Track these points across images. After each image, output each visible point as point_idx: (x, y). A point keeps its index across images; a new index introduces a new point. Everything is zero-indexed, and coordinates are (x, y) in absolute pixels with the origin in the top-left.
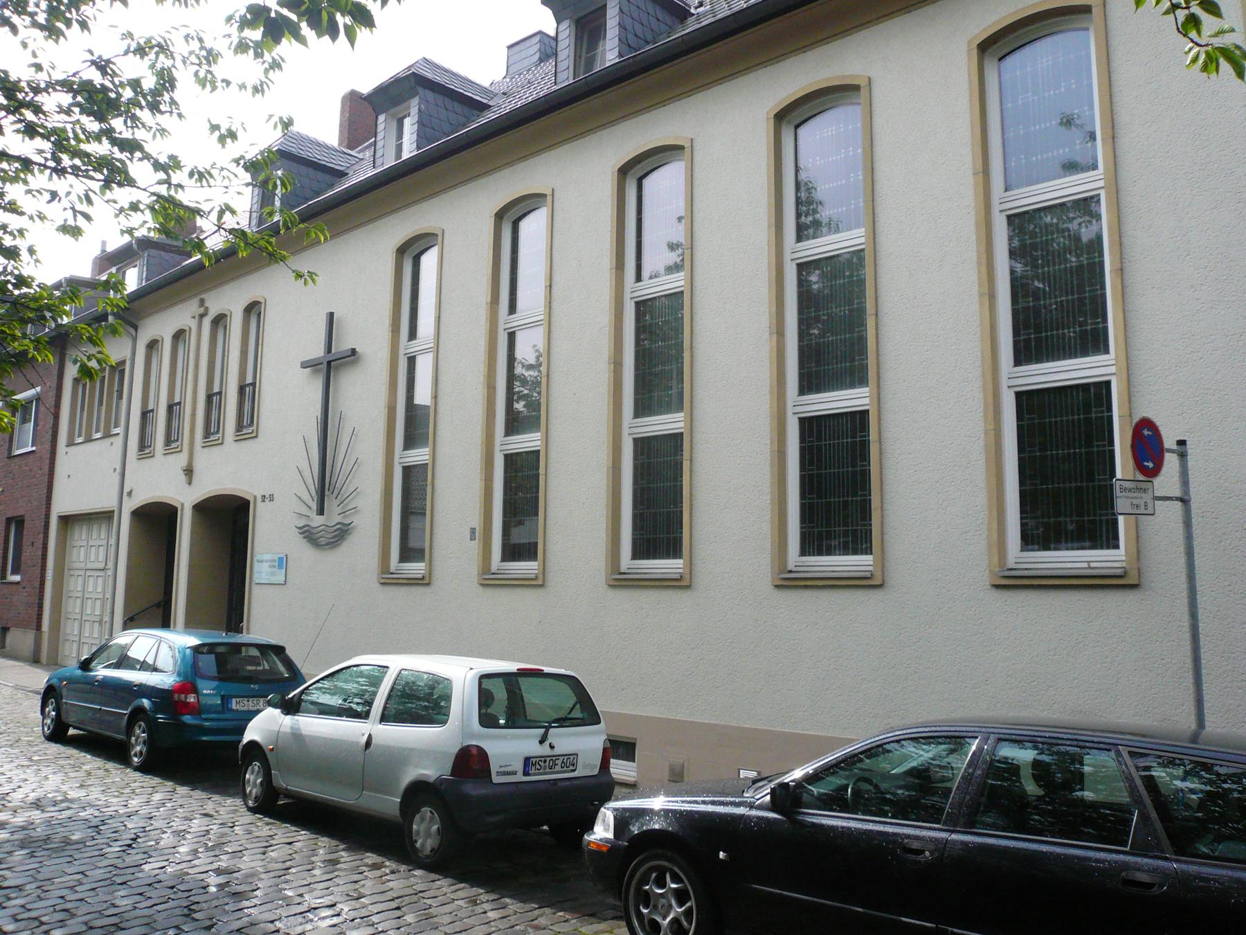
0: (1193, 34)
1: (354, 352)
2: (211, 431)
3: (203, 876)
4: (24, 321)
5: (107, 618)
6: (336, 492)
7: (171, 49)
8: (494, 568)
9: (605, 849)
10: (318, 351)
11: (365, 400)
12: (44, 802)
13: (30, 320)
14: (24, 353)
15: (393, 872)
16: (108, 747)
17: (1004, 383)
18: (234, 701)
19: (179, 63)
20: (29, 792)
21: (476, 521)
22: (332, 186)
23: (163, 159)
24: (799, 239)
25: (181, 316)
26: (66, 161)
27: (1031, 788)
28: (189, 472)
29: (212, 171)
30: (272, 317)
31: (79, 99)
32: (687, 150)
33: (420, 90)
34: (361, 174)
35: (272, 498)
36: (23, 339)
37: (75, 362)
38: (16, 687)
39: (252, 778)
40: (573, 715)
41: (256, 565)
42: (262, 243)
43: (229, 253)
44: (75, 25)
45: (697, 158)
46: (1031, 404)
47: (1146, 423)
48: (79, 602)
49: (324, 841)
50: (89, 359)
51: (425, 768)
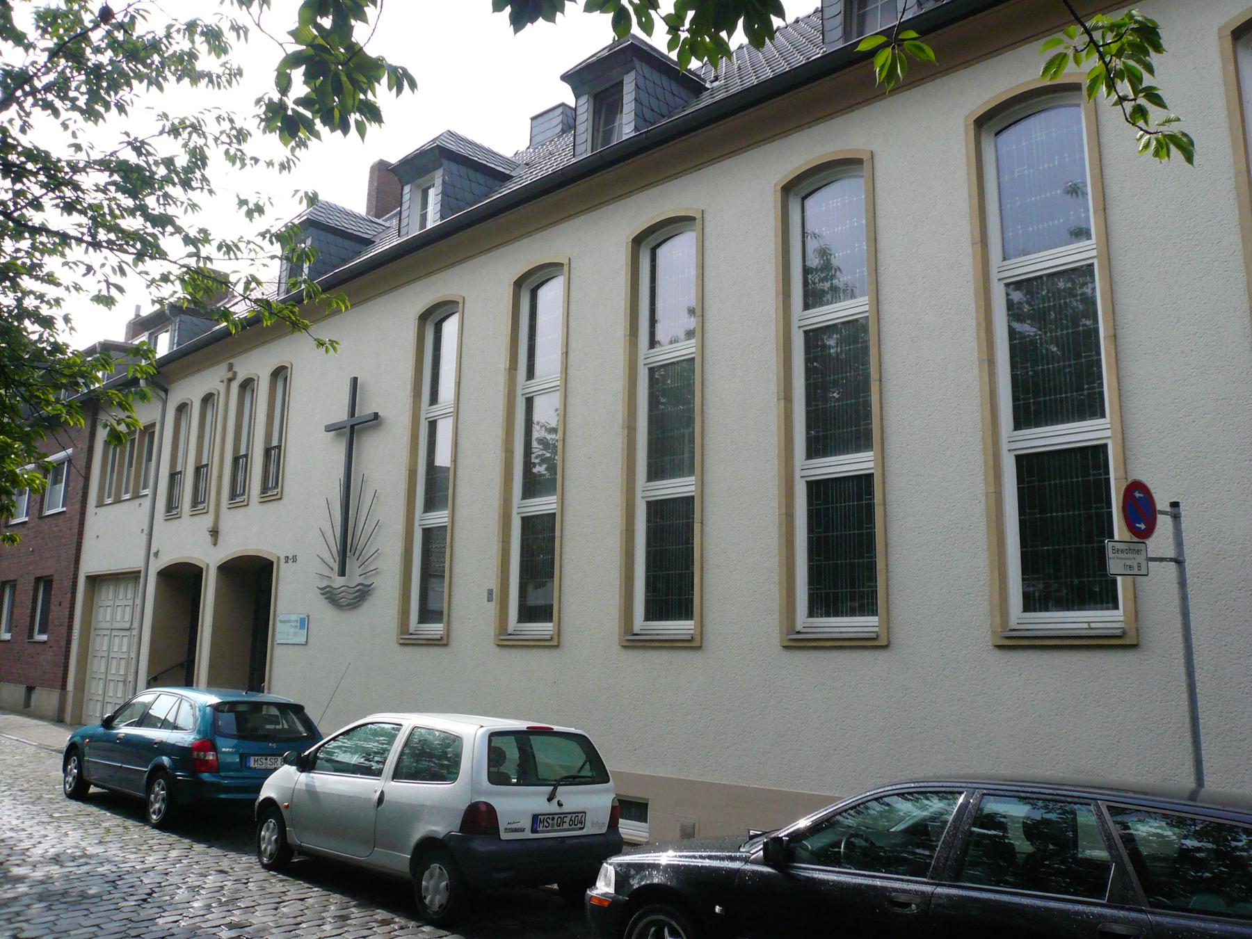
0: (1141, 123)
1: (376, 416)
2: (237, 493)
3: (215, 930)
4: (58, 387)
5: (131, 678)
6: (357, 553)
7: (204, 129)
8: (510, 629)
9: (606, 904)
10: (342, 415)
11: (386, 461)
12: (62, 858)
13: (63, 386)
14: (58, 417)
15: (402, 928)
16: (127, 805)
17: (1005, 446)
18: (252, 759)
19: (211, 142)
20: (49, 847)
21: (493, 583)
22: (359, 254)
23: (193, 233)
24: (807, 306)
25: (210, 380)
26: (102, 235)
27: (1022, 845)
28: (215, 533)
29: (240, 245)
30: (299, 383)
31: (116, 177)
32: (698, 222)
33: (445, 162)
34: (388, 243)
35: (295, 559)
36: (56, 402)
37: (105, 426)
38: (40, 746)
39: (267, 834)
40: (582, 774)
41: (279, 625)
42: (286, 312)
43: (252, 322)
44: (114, 110)
45: (707, 230)
46: (1031, 467)
47: (1137, 486)
48: (104, 661)
49: (336, 898)
50: (119, 424)
51: (434, 824)
